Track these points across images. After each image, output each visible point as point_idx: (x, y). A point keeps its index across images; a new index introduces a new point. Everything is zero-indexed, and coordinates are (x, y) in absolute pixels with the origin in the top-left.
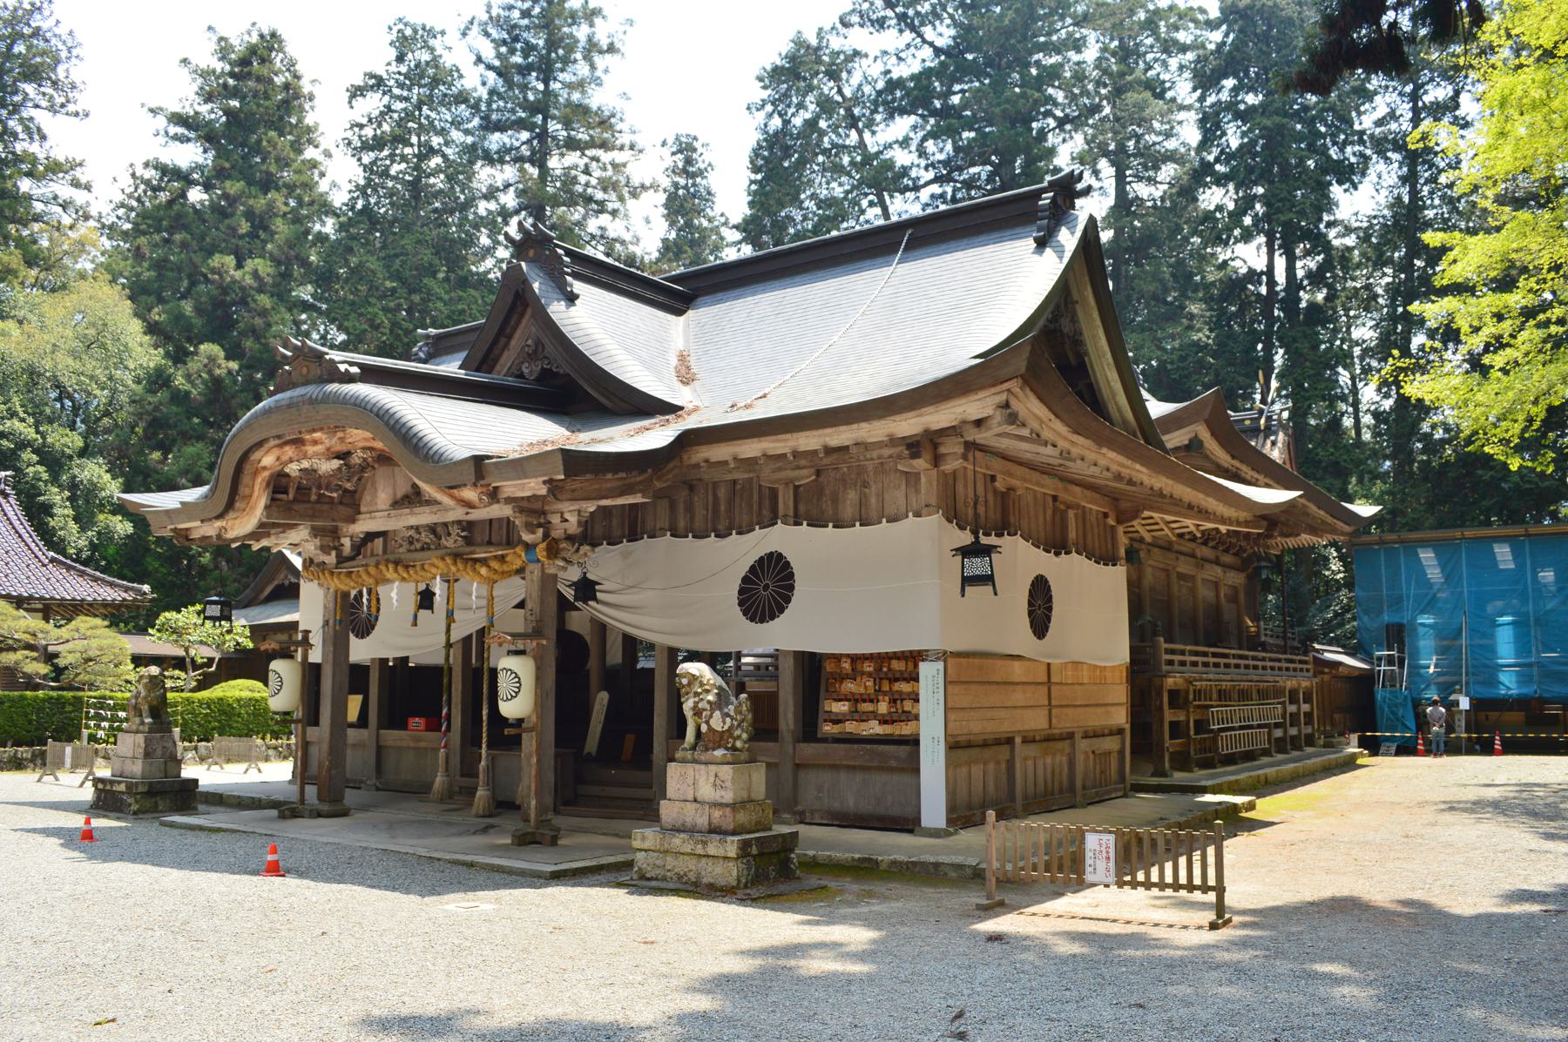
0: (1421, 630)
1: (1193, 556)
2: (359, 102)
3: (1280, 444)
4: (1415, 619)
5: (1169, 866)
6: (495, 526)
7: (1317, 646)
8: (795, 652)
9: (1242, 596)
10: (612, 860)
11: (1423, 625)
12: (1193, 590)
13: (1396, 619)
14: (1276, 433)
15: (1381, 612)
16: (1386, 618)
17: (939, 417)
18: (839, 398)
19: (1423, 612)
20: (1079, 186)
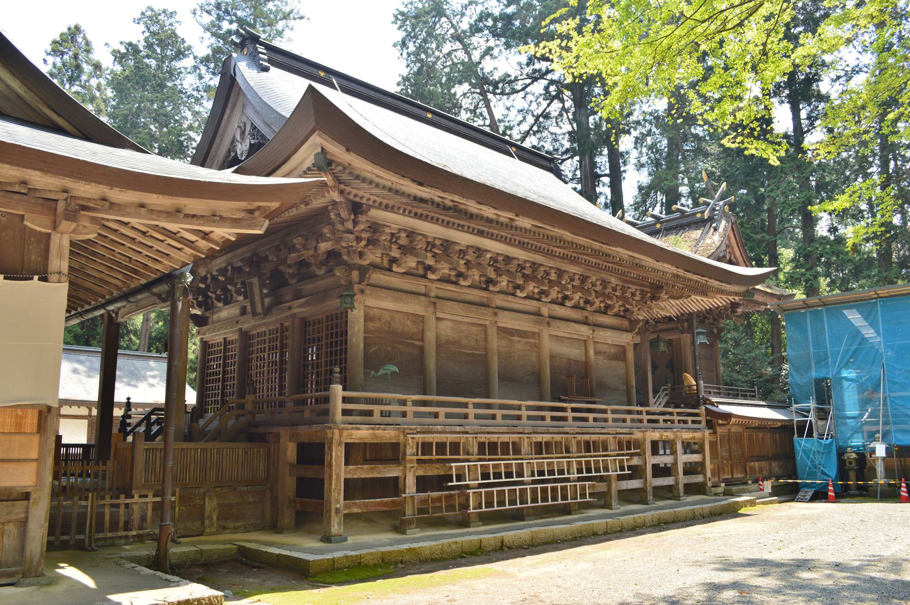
0: (846, 384)
1: (538, 314)
2: (56, 198)
3: (721, 230)
4: (839, 372)
5: (265, 57)
6: (74, 293)
7: (714, 400)
9: (630, 355)
10: (559, 232)
11: (846, 379)
12: (538, 347)
13: (822, 374)
14: (719, 221)
15: (808, 370)
16: (814, 374)
17: (423, 540)
18: (659, 536)
19: (846, 366)
20: (101, 462)
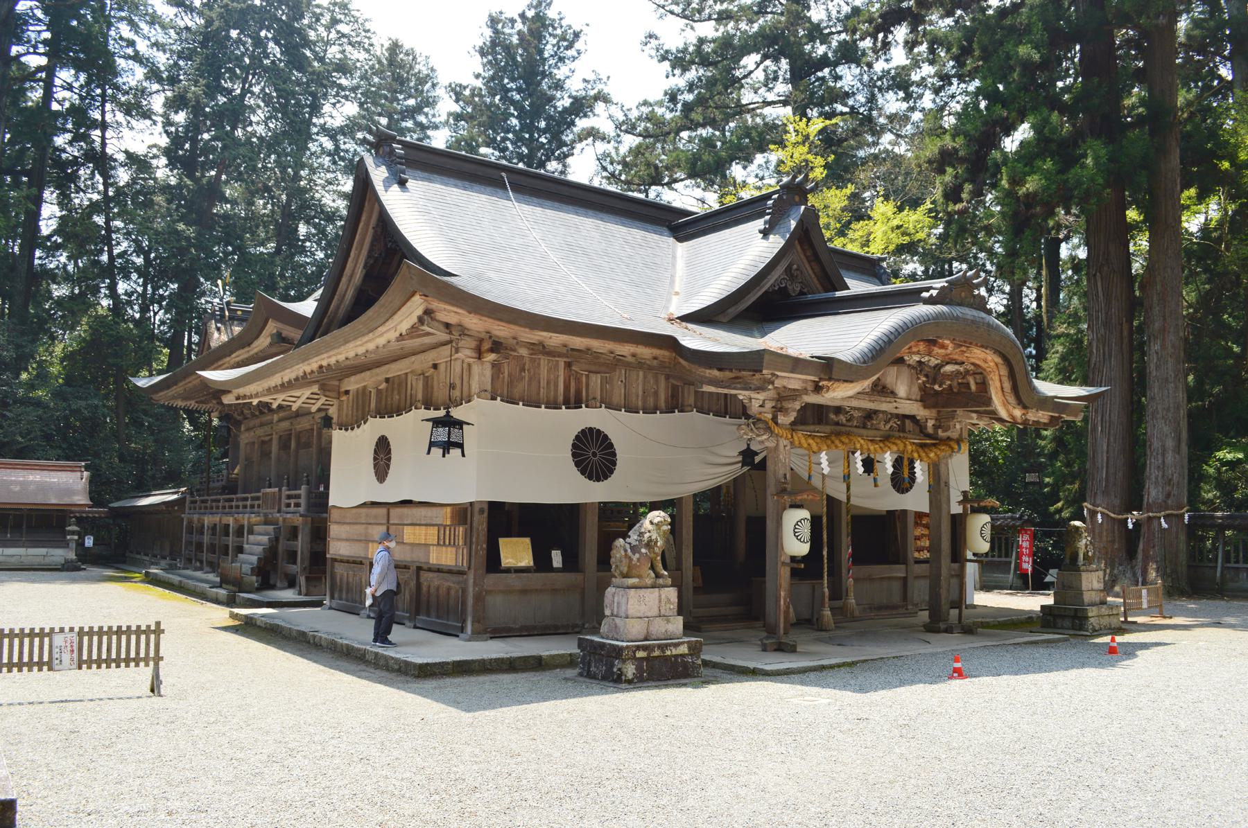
8: (491, 504)
